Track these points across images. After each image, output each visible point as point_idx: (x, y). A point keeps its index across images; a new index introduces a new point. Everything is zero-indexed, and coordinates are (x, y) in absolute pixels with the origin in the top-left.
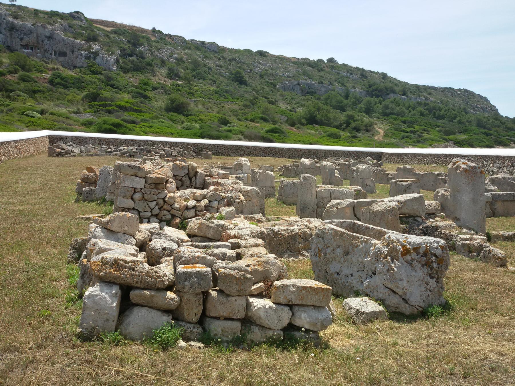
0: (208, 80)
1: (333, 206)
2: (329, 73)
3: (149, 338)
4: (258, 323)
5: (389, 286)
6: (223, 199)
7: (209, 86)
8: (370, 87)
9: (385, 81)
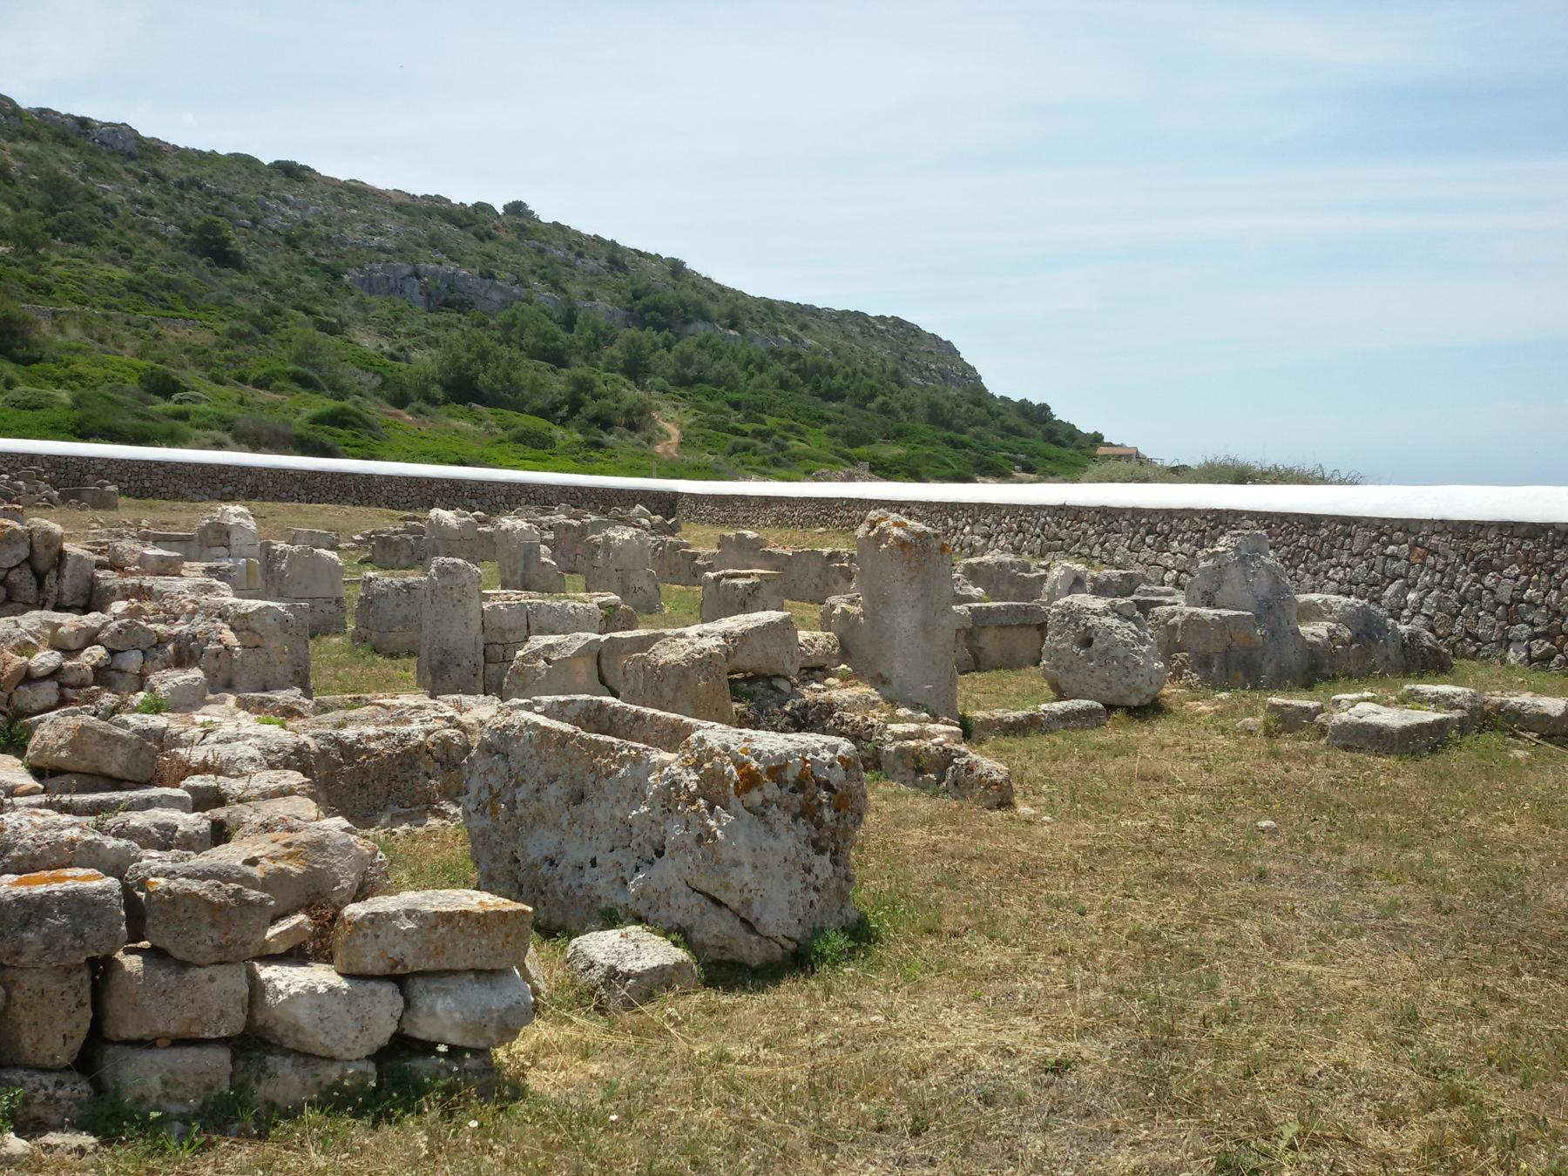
1: (536, 655)
2: (511, 246)
5: (703, 886)
7: (108, 266)
8: (637, 297)
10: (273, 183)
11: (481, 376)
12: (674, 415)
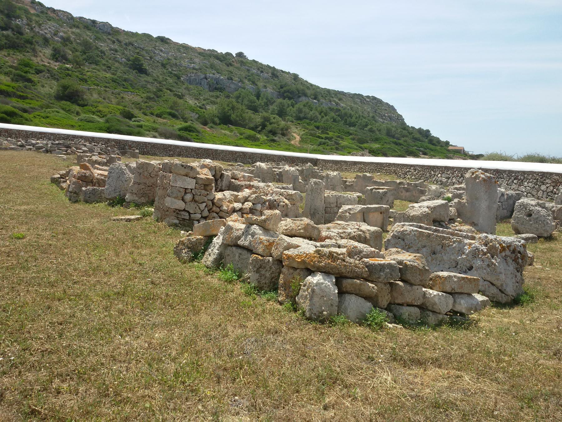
0: (102, 66)
1: (346, 211)
2: (238, 68)
3: (362, 321)
4: (430, 308)
5: (489, 279)
6: (264, 203)
7: (104, 73)
8: (282, 88)
9: (296, 83)
10: (157, 44)
11: (232, 115)
12: (296, 130)
